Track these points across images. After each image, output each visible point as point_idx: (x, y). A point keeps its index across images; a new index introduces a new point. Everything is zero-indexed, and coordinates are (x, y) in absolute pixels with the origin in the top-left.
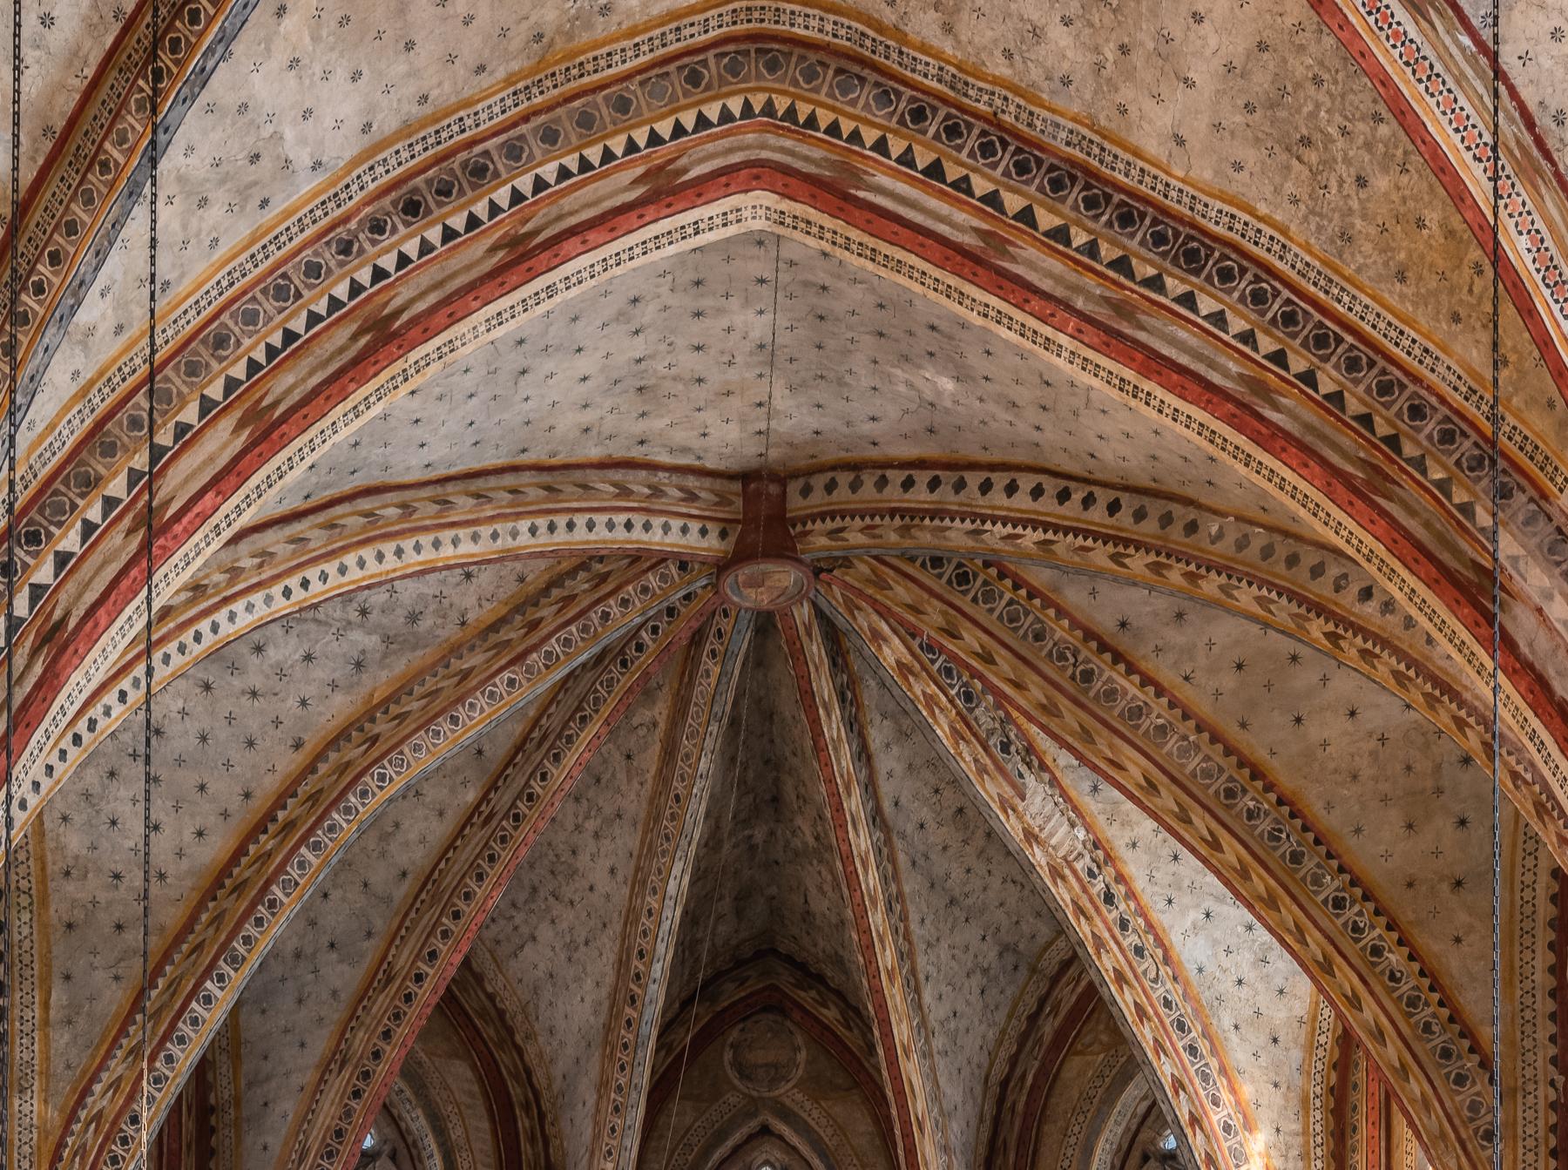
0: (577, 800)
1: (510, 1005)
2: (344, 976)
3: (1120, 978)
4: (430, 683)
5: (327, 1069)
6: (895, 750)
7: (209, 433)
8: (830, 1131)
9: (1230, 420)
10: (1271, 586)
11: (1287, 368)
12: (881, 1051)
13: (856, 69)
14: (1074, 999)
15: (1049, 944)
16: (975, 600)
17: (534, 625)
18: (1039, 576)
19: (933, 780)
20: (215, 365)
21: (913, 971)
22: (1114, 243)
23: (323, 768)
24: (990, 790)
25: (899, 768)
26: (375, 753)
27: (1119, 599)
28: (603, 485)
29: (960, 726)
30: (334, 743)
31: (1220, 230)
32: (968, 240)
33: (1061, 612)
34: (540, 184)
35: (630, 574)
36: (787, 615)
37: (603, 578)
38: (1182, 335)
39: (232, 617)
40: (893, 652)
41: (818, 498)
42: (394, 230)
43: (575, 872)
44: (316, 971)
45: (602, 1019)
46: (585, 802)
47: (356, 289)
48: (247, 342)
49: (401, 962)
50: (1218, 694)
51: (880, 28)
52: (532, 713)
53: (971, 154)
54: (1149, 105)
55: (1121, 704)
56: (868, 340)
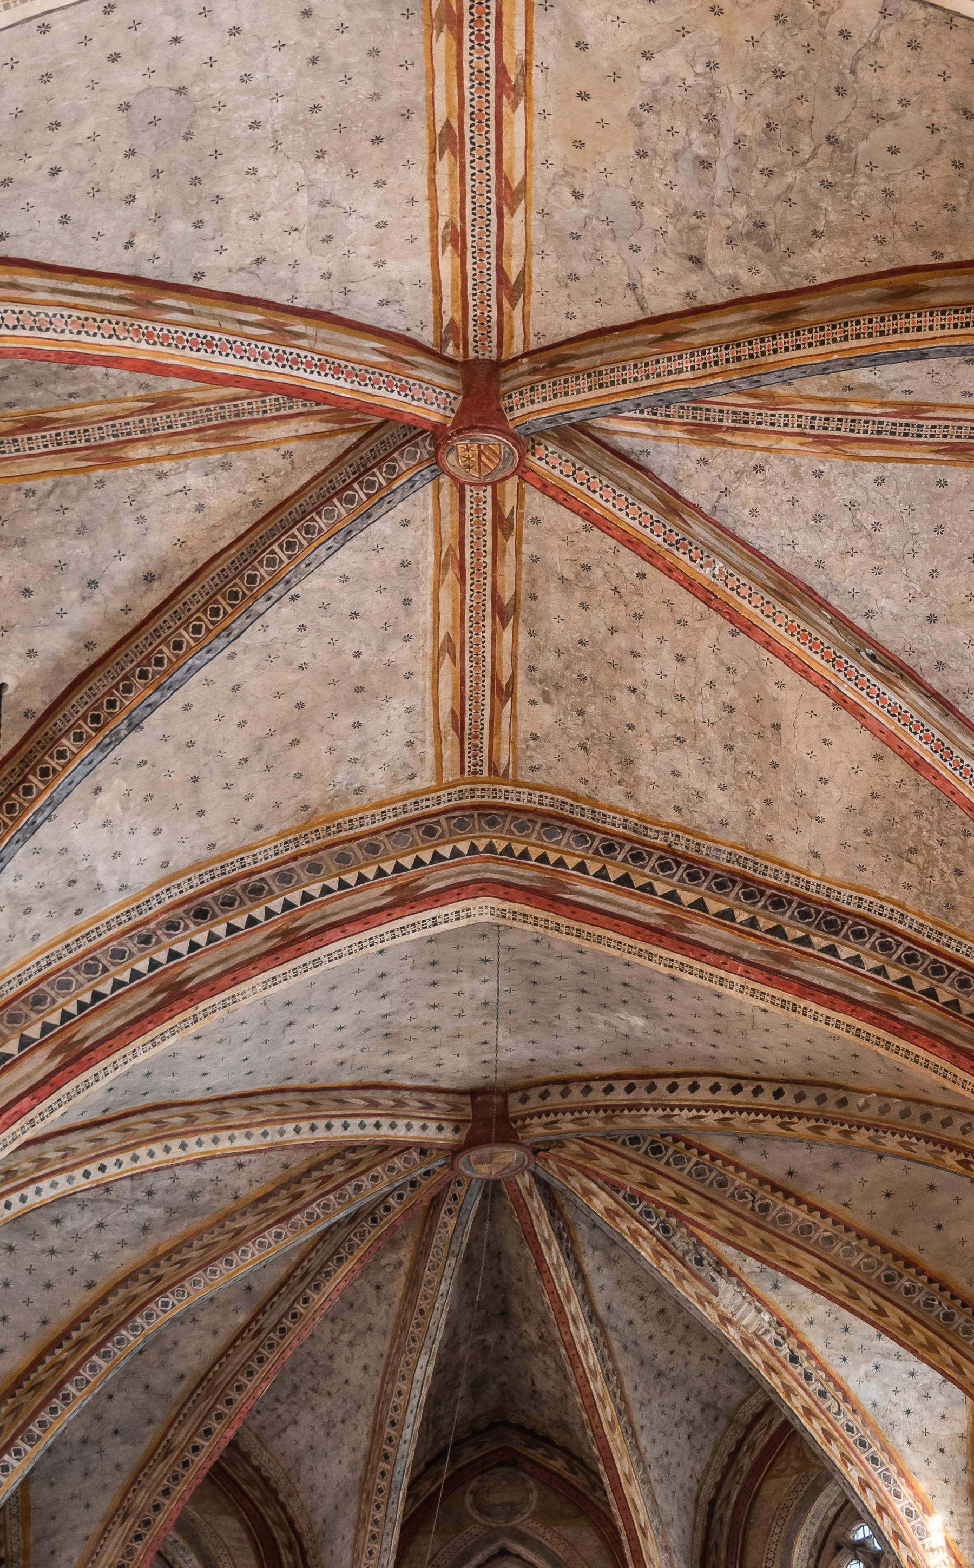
0: (333, 1320)
1: (273, 1473)
2: (127, 1454)
3: (808, 1413)
4: (207, 1239)
5: (111, 1521)
6: (605, 1271)
7: (27, 1060)
8: (562, 1548)
9: (871, 1021)
10: (910, 1135)
11: (912, 987)
12: (606, 1480)
13: (559, 823)
14: (767, 1439)
15: (742, 1402)
16: (668, 1163)
17: (297, 1196)
18: (720, 1144)
19: (639, 1291)
20: (33, 1016)
21: (630, 1423)
22: (769, 918)
23: (112, 1300)
24: (688, 1291)
25: (609, 1284)
26: (159, 1287)
27: (787, 1155)
28: (356, 1100)
29: (660, 1248)
30: (123, 1282)
31: (851, 908)
32: (653, 921)
33: (739, 1168)
34: (306, 897)
35: (379, 1158)
36: (512, 1182)
37: (356, 1163)
38: (828, 971)
39: (38, 1192)
40: (601, 1202)
41: (534, 1102)
42: (186, 927)
43: (332, 1371)
44: (101, 1451)
45: (358, 1474)
46: (340, 1322)
47: (153, 965)
48: (61, 1001)
49: (179, 1439)
50: (872, 1213)
51: (576, 798)
52: (295, 1258)
53: (653, 870)
54: (790, 835)
55: (793, 1225)
56: (573, 997)
